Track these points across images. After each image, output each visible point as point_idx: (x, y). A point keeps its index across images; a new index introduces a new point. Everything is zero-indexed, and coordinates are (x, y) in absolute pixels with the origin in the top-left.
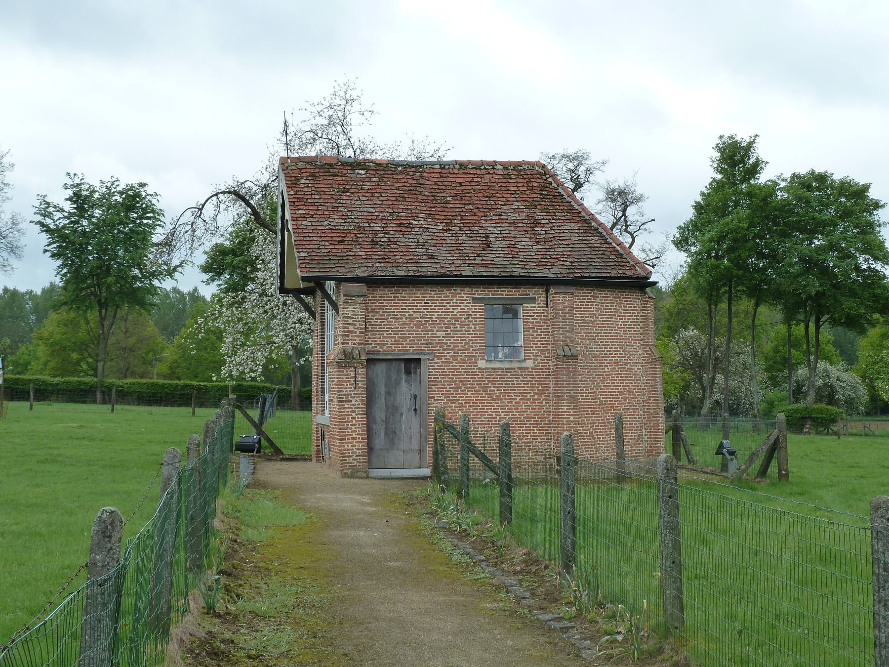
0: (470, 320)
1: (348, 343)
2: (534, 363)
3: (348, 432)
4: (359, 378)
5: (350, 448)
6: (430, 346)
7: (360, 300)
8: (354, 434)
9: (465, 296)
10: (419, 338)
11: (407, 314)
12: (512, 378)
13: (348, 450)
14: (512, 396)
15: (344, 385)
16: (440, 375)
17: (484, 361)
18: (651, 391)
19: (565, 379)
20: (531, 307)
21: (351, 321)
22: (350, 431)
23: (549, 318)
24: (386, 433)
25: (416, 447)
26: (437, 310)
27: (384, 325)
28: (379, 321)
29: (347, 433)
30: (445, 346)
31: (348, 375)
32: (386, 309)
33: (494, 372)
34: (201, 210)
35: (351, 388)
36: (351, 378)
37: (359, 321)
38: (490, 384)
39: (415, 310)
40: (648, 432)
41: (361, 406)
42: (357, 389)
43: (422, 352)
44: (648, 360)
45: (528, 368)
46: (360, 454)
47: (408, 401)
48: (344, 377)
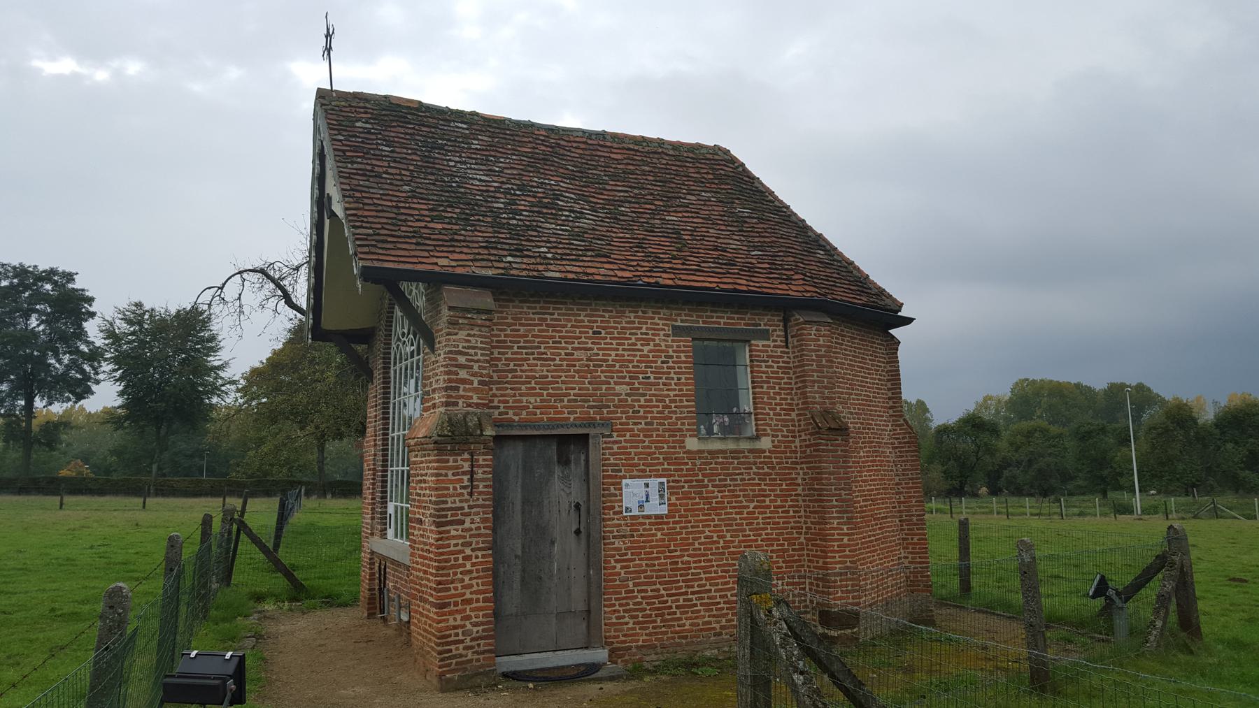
2: (773, 441)
3: (456, 589)
4: (480, 475)
5: (459, 622)
6: (605, 411)
7: (480, 319)
8: (468, 592)
9: (661, 322)
11: (563, 352)
12: (740, 469)
13: (455, 627)
14: (741, 502)
15: (448, 489)
16: (623, 465)
18: (911, 488)
19: (832, 469)
20: (763, 346)
21: (462, 360)
22: (459, 585)
23: (791, 365)
24: (523, 580)
25: (581, 607)
26: (614, 346)
27: (522, 371)
28: (512, 364)
29: (453, 592)
30: (631, 411)
31: (457, 468)
32: (526, 342)
33: (713, 458)
34: (221, 288)
35: (462, 494)
36: (464, 473)
37: (478, 361)
38: (706, 479)
39: (576, 345)
40: (908, 553)
41: (483, 531)
42: (475, 497)
43: (591, 424)
44: (903, 438)
45: (764, 451)
46: (481, 633)
47: (564, 514)
48: (450, 473)
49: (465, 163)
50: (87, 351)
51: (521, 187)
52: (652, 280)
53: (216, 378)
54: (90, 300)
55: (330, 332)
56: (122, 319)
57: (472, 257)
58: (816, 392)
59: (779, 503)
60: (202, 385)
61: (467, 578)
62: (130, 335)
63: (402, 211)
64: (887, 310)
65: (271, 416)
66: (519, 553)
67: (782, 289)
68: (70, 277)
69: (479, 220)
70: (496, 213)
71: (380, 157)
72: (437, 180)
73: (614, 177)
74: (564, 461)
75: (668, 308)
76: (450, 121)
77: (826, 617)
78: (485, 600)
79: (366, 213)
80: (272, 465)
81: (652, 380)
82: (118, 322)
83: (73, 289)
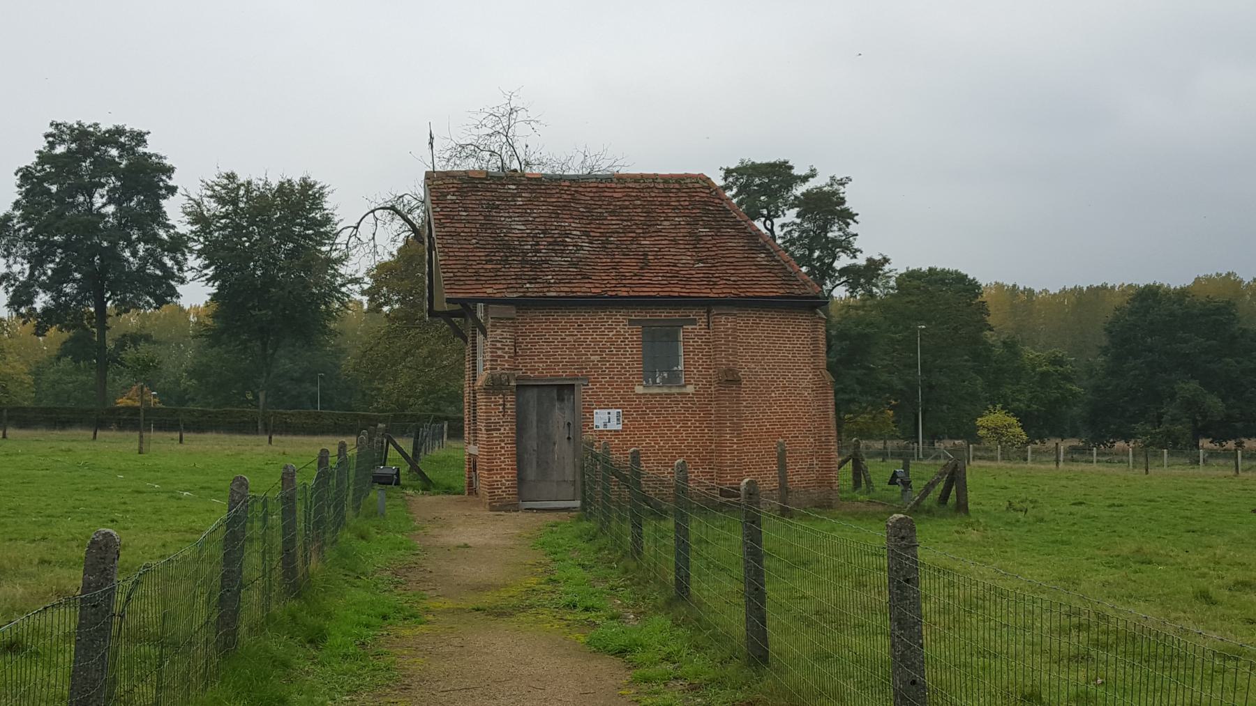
0: (627, 343)
1: (496, 369)
4: (508, 406)
6: (584, 371)
8: (503, 464)
10: (572, 363)
13: (497, 481)
17: (642, 387)
21: (499, 345)
24: (538, 465)
34: (357, 228)
36: (500, 405)
39: (567, 333)
47: (561, 429)
49: (511, 217)
50: (166, 238)
51: (544, 232)
52: (614, 293)
53: (333, 276)
54: (169, 171)
55: (439, 312)
56: (211, 197)
57: (505, 286)
58: (723, 358)
59: (698, 425)
60: (316, 285)
61: (502, 458)
62: (223, 218)
63: (471, 258)
64: (807, 298)
65: (405, 319)
66: (536, 448)
67: (706, 292)
68: (139, 138)
69: (514, 260)
70: (525, 253)
71: (460, 221)
72: (492, 233)
73: (612, 213)
74: (561, 399)
75: (626, 309)
76: (505, 185)
77: (723, 493)
78: (512, 469)
79: (451, 262)
80: (410, 397)
81: (614, 352)
82: (206, 200)
83: (145, 153)
